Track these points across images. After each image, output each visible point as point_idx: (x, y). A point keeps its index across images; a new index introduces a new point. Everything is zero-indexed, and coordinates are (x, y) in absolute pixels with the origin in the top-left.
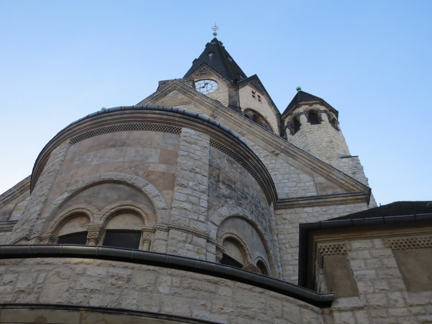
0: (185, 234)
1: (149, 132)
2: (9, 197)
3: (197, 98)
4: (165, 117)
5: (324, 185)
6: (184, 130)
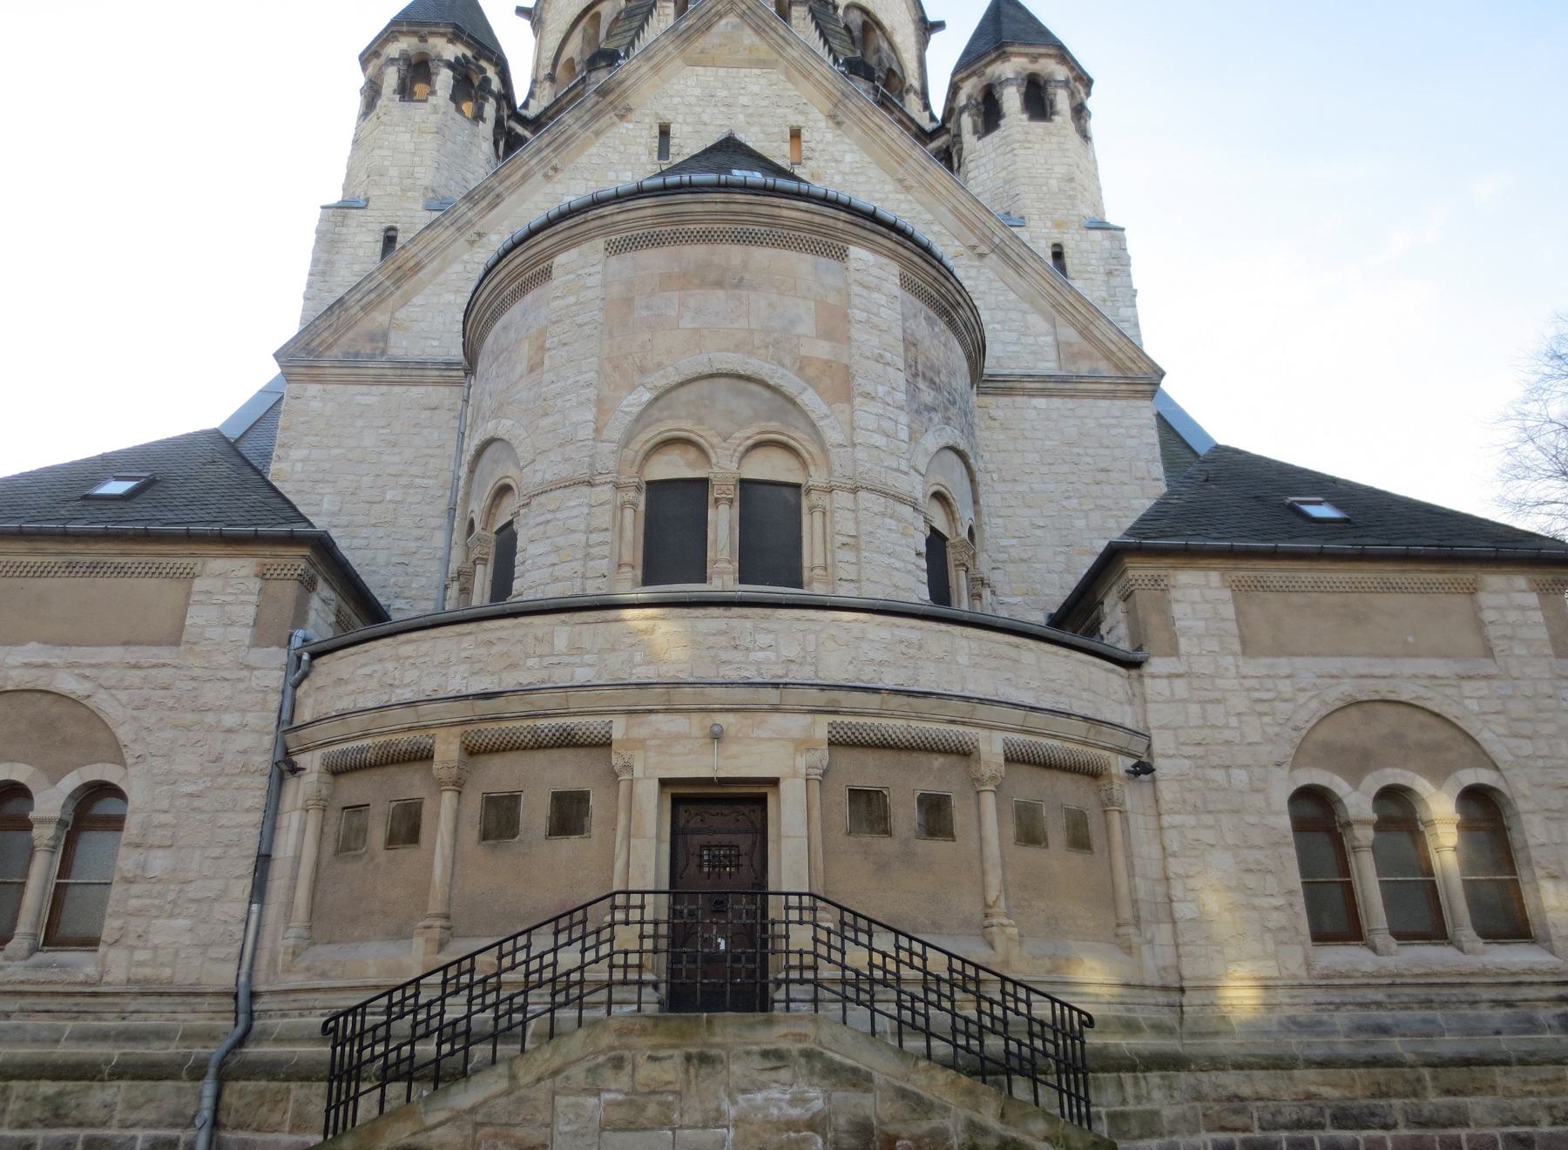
0: (882, 500)
1: (788, 253)
2: (373, 295)
3: (795, 54)
4: (817, 219)
5: (1075, 349)
6: (855, 252)
